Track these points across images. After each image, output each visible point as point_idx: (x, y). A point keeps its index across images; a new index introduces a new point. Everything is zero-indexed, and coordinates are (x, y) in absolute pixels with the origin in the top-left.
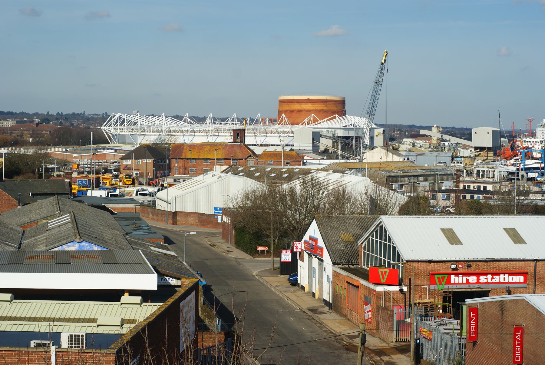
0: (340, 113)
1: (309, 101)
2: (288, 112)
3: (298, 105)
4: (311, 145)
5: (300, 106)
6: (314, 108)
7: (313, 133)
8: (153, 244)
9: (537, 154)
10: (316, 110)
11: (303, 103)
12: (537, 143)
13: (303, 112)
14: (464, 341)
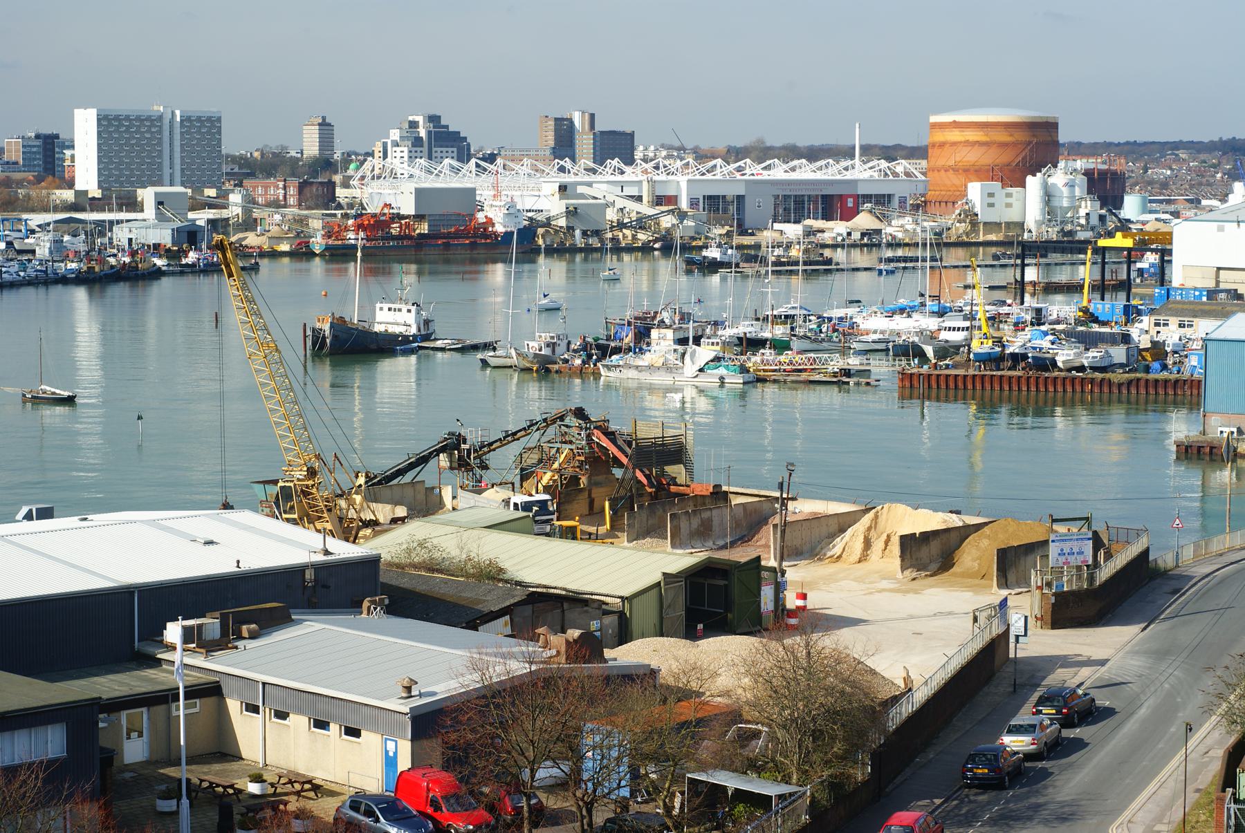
0: (1020, 146)
1: (956, 125)
4: (154, 211)
7: (156, 194)
10: (967, 141)
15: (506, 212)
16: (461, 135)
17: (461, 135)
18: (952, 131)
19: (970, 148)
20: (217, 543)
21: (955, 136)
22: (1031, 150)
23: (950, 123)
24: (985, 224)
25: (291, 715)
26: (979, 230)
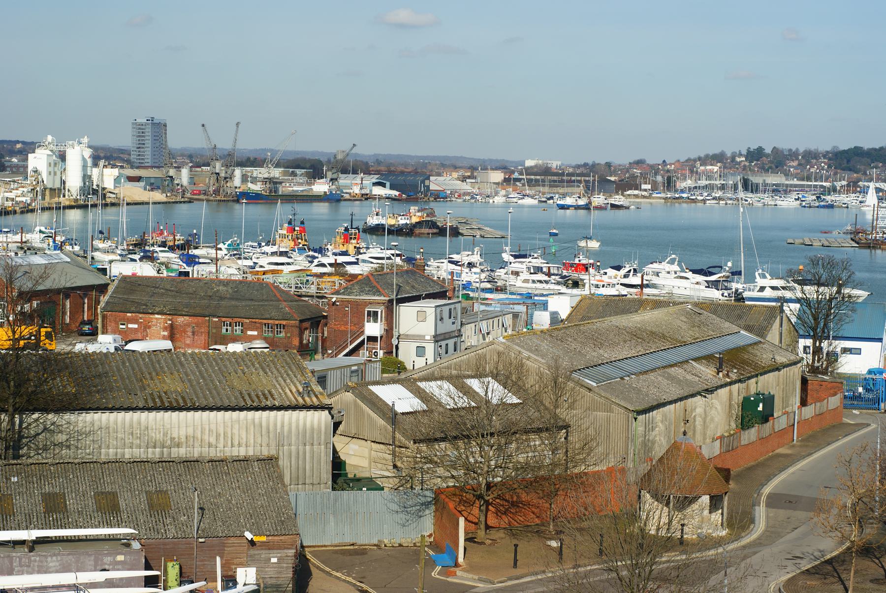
24: (51, 189)
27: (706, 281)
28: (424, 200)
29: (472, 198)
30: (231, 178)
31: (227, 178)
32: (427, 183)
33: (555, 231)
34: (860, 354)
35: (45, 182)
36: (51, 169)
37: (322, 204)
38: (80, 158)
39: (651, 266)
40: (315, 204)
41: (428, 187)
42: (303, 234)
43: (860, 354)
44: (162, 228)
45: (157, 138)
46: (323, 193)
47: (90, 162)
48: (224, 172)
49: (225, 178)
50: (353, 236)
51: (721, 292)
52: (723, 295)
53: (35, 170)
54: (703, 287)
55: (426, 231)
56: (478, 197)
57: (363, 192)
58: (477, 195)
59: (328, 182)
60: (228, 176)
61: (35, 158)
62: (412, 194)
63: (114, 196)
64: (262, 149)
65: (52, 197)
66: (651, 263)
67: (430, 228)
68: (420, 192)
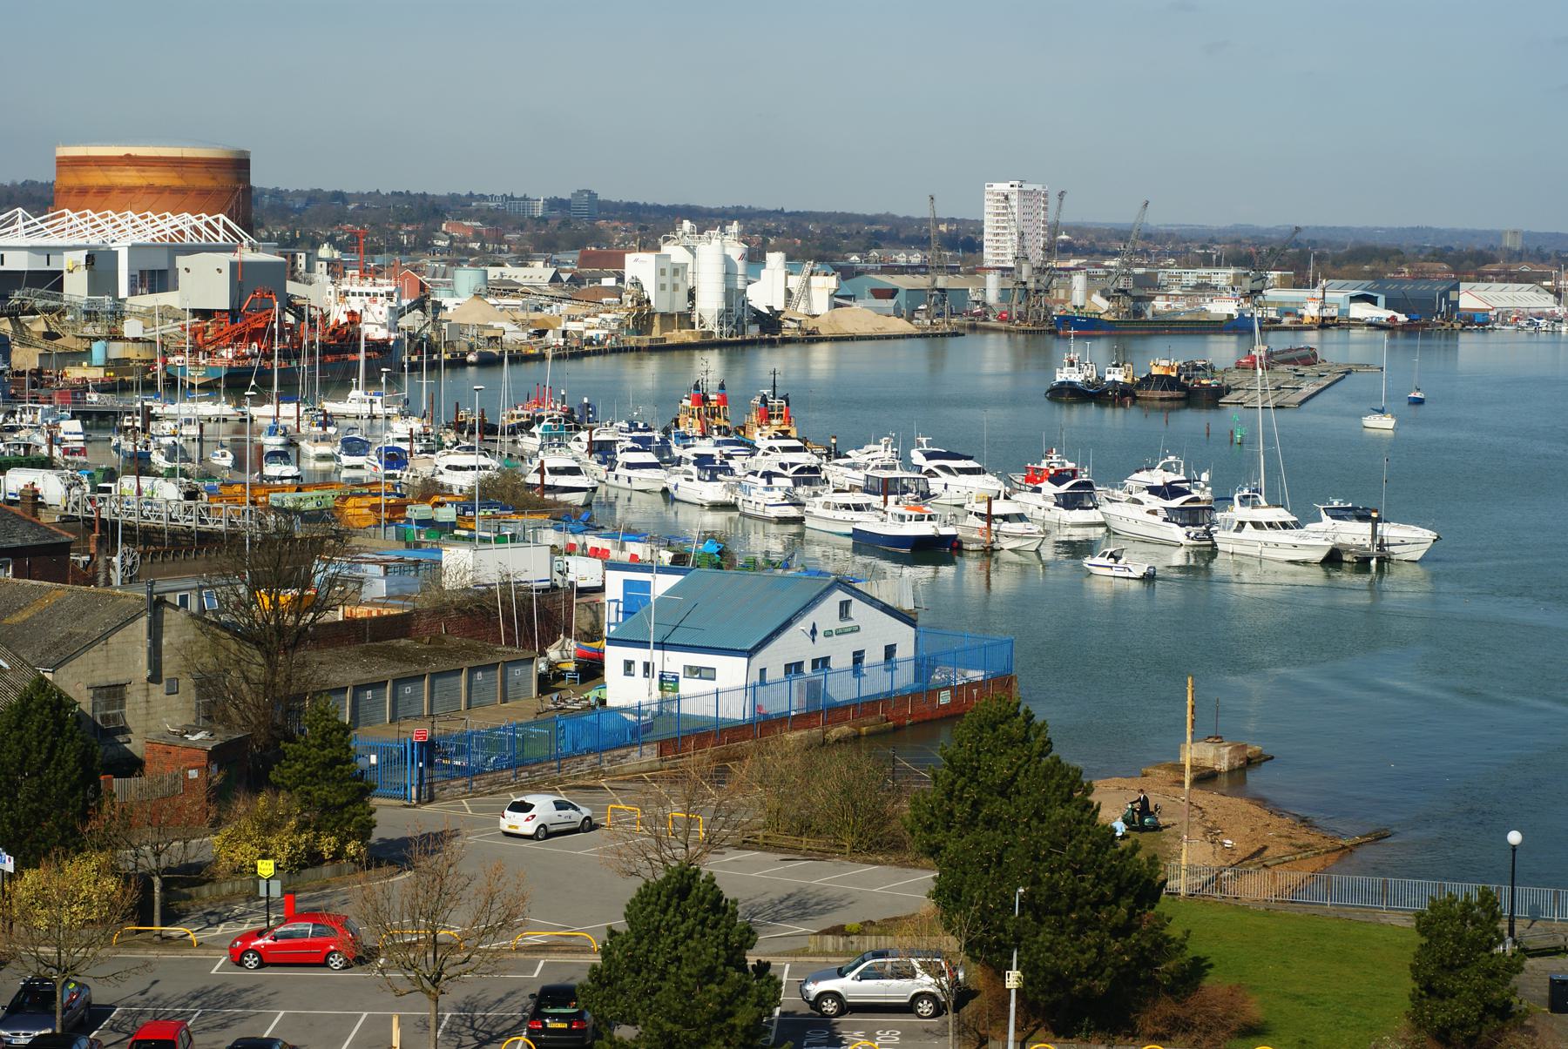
1: (129, 160)
2: (73, 193)
3: (101, 173)
5: (106, 176)
6: (144, 182)
8: (557, 504)
9: (376, 330)
11: (114, 168)
12: (379, 299)
13: (115, 193)
14: (242, 858)
15: (393, 304)
16: (291, 191)
17: (291, 191)
18: (123, 171)
19: (156, 196)
20: (814, 624)
21: (129, 177)
22: (238, 202)
23: (121, 157)
24: (663, 315)
25: (1095, 783)
26: (651, 325)
27: (1165, 508)
28: (1444, 327)
29: (1531, 323)
30: (1047, 291)
31: (1040, 291)
32: (1453, 296)
33: (1418, 395)
34: (714, 679)
35: (653, 303)
36: (666, 280)
37: (1224, 338)
38: (719, 260)
39: (1135, 476)
40: (1213, 338)
41: (1457, 303)
42: (722, 407)
43: (714, 679)
44: (563, 393)
45: (1027, 217)
46: (1226, 317)
47: (741, 266)
48: (1033, 280)
49: (1037, 291)
50: (776, 413)
51: (1184, 530)
52: (1188, 535)
53: (634, 281)
54: (1158, 520)
55: (1158, 394)
56: (1541, 321)
57: (1325, 313)
58: (1539, 319)
59: (1237, 296)
60: (1041, 287)
61: (636, 260)
62: (1416, 316)
63: (795, 325)
64: (1413, 229)
65: (664, 328)
66: (1137, 472)
67: (1164, 389)
68: (1439, 312)
